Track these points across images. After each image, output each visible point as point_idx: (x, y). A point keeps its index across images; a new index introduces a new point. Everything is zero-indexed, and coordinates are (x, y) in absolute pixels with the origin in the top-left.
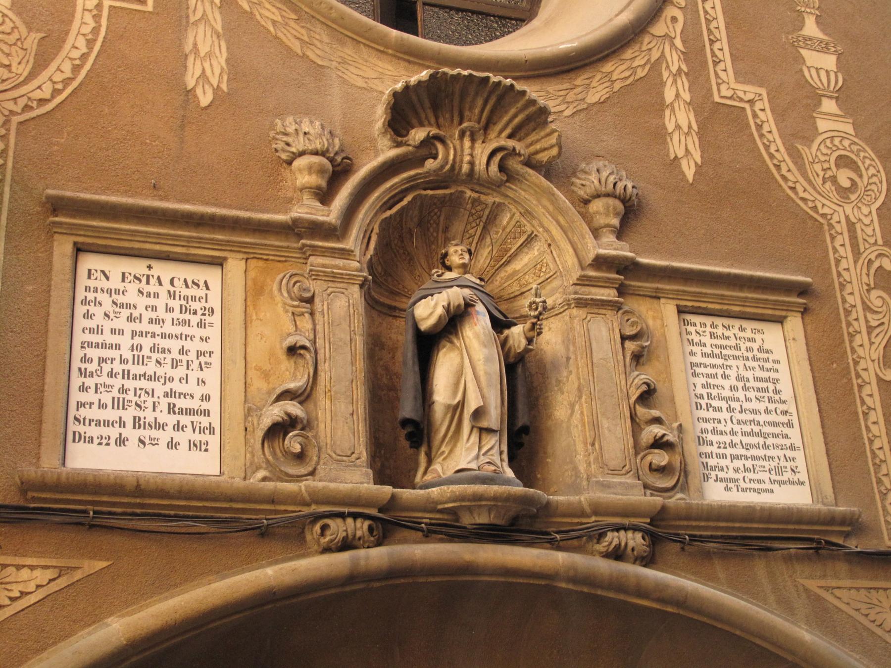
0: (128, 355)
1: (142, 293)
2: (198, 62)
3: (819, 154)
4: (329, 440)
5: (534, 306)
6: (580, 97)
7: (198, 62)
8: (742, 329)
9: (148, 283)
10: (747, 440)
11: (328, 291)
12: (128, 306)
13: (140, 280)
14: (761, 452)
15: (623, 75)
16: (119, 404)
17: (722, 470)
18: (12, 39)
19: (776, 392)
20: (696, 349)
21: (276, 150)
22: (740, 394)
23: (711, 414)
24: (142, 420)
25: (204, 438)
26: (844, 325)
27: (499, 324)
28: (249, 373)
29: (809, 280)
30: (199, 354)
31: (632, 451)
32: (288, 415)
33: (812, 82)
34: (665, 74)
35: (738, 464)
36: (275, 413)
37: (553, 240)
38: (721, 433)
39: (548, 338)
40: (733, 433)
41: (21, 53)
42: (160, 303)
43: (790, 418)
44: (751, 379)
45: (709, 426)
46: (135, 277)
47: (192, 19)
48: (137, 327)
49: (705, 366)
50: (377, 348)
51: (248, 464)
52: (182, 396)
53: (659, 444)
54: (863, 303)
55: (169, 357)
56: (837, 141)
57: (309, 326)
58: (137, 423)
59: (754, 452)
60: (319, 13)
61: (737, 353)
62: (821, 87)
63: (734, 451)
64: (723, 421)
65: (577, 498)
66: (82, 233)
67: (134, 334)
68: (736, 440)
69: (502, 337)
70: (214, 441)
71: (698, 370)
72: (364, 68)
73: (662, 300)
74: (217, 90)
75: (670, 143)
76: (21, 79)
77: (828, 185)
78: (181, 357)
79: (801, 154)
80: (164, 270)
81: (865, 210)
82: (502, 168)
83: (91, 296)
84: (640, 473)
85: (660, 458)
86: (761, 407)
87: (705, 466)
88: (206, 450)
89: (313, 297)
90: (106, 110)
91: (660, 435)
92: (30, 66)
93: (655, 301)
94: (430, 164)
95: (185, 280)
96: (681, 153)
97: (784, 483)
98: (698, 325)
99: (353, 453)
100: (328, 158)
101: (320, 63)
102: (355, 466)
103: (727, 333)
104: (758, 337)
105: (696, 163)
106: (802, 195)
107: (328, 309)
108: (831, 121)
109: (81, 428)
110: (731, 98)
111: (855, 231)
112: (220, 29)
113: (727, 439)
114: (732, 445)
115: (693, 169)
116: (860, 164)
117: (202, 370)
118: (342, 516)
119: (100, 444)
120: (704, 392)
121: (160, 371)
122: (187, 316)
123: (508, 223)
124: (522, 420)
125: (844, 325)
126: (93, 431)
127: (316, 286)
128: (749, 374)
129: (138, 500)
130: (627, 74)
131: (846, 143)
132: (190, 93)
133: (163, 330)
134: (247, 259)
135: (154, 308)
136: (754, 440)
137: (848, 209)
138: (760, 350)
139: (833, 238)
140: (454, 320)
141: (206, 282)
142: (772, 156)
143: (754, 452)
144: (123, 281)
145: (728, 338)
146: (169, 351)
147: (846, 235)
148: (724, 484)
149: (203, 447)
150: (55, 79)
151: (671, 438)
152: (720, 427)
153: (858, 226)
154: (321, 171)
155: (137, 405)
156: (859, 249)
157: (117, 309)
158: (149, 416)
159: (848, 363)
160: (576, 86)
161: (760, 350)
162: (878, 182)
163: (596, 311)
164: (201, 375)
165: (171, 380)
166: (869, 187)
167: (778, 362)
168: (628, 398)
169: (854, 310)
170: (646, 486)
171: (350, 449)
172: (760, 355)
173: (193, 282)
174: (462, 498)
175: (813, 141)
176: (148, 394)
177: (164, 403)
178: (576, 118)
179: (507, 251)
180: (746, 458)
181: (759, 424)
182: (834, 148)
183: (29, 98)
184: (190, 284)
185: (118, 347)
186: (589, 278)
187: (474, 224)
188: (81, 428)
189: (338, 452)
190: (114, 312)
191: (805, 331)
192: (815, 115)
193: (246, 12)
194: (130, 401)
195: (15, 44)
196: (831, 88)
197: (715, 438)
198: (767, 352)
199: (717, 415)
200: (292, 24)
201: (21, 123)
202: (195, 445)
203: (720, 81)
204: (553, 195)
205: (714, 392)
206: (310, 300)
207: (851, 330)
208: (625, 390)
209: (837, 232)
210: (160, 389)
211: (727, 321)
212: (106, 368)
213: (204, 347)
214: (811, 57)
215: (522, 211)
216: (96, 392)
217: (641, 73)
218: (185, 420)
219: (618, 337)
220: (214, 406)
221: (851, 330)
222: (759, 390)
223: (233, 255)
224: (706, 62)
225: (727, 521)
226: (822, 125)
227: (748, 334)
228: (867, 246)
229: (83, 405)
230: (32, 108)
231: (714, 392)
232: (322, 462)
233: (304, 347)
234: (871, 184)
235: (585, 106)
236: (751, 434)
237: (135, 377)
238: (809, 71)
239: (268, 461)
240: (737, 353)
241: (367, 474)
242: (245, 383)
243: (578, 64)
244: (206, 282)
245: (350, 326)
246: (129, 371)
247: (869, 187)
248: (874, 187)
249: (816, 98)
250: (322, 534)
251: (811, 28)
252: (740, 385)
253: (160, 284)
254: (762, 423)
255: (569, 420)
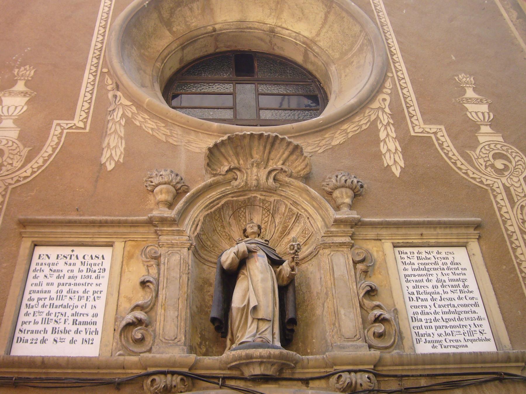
0: (54, 295)
1: (67, 264)
2: (109, 151)
3: (481, 154)
4: (161, 332)
5: (292, 247)
6: (328, 143)
7: (109, 151)
8: (438, 253)
9: (71, 258)
10: (445, 316)
11: (169, 253)
12: (58, 271)
13: (66, 258)
14: (457, 323)
15: (354, 129)
16: (45, 321)
17: (430, 335)
18: (16, 152)
19: (465, 286)
20: (407, 267)
21: (146, 186)
22: (440, 290)
23: (420, 303)
24: (57, 329)
25: (91, 337)
26: (508, 243)
27: (275, 262)
28: (120, 299)
29: (480, 219)
30: (94, 292)
31: (361, 326)
32: (137, 318)
33: (473, 119)
34: (380, 126)
35: (440, 331)
36: (130, 318)
37: (310, 215)
38: (428, 314)
39: (311, 270)
40: (436, 313)
41: (19, 157)
42: (76, 269)
43: (476, 301)
44: (447, 280)
45: (419, 310)
46: (64, 256)
47: (109, 132)
48: (61, 281)
49: (415, 276)
50: (206, 286)
51: (114, 349)
52: (82, 315)
53: (378, 320)
54: (520, 229)
55: (77, 295)
56: (492, 146)
57: (156, 271)
58: (54, 331)
59: (452, 323)
60: (177, 121)
61: (436, 267)
62: (479, 120)
63: (437, 324)
64: (428, 307)
65: (321, 356)
66: (36, 236)
67: (59, 285)
68: (438, 317)
69: (278, 270)
70: (97, 339)
71: (409, 278)
72: (200, 143)
73: (383, 241)
74: (117, 163)
75: (384, 159)
76: (17, 169)
77: (489, 169)
78: (84, 295)
79: (469, 155)
80: (80, 251)
81: (516, 179)
82: (275, 179)
83: (38, 267)
84: (367, 338)
85: (380, 328)
86: (455, 296)
87: (417, 334)
88: (92, 343)
89: (160, 256)
90: (58, 178)
91: (378, 314)
92: (22, 162)
93: (378, 242)
94: (235, 183)
95: (91, 256)
96: (391, 163)
97: (475, 340)
98: (409, 253)
99: (176, 338)
100: (172, 186)
101: (175, 144)
102: (177, 345)
103: (428, 256)
104: (450, 256)
105: (401, 167)
106: (471, 175)
107: (168, 261)
108: (486, 136)
109: (22, 335)
110: (422, 132)
111: (510, 191)
112: (123, 136)
113: (432, 317)
114: (436, 320)
115: (399, 170)
116: (509, 156)
117: (95, 300)
118: (165, 373)
119: (32, 343)
120: (414, 291)
121: (71, 303)
122: (90, 274)
123: (285, 211)
124: (290, 314)
125: (508, 243)
126: (29, 336)
127: (162, 251)
128: (445, 278)
129: (44, 371)
130: (356, 128)
131: (499, 146)
132: (102, 166)
133: (76, 282)
134: (125, 241)
135: (72, 271)
136: (452, 316)
137: (504, 180)
138: (452, 263)
139: (495, 197)
140: (243, 261)
141: (103, 256)
142: (450, 158)
143: (452, 323)
144: (57, 258)
145: (429, 259)
146: (78, 292)
147: (504, 194)
148: (432, 344)
149: (91, 342)
150: (33, 167)
151: (387, 316)
152: (427, 310)
153: (512, 189)
154: (168, 192)
155: (55, 321)
156: (514, 201)
157: (52, 273)
158: (61, 327)
159: (514, 265)
160: (325, 138)
161: (452, 263)
162: (522, 164)
163: (337, 249)
164: (94, 303)
165: (77, 307)
166: (517, 167)
167: (465, 269)
168: (358, 295)
169: (514, 234)
170: (370, 347)
171: (174, 336)
172: (452, 266)
173: (96, 256)
174: (240, 358)
175: (476, 148)
176: (62, 315)
177: (71, 319)
178: (326, 153)
179: (287, 227)
180: (446, 327)
181: (454, 306)
182: (491, 150)
183: (19, 177)
184: (94, 257)
185: (49, 292)
186: (332, 232)
187: (266, 215)
188: (22, 335)
189: (166, 338)
190: (50, 275)
191: (481, 249)
192: (477, 135)
193: (138, 126)
194: (52, 320)
195: (16, 154)
196: (486, 120)
197: (423, 317)
198: (457, 264)
199: (424, 303)
200: (162, 128)
201: (13, 188)
202: (86, 341)
203: (414, 125)
204: (308, 190)
205: (421, 290)
206: (157, 258)
207: (514, 246)
208: (356, 291)
209: (498, 193)
210: (69, 312)
211: (428, 249)
212: (41, 303)
213: (98, 289)
214: (471, 107)
215: (291, 202)
216: (34, 316)
217: (364, 127)
218: (82, 328)
219: (351, 262)
220: (100, 320)
221: (514, 246)
222: (452, 286)
223: (118, 240)
224: (405, 117)
225: (431, 364)
226: (482, 139)
227: (443, 255)
228: (519, 198)
229: (25, 323)
230: (20, 181)
231: (421, 290)
232: (156, 344)
233: (148, 281)
234: (518, 165)
235: (331, 147)
236: (449, 312)
237: (56, 307)
238: (471, 114)
239: (123, 345)
240: (436, 267)
241: (183, 350)
242: (117, 305)
243: (324, 127)
244: (103, 256)
245: (180, 270)
246: (53, 304)
247: (517, 167)
248: (520, 167)
249: (477, 127)
250: (152, 385)
251: (470, 93)
252: (439, 284)
253: (77, 258)
254: (456, 305)
255: (322, 313)
